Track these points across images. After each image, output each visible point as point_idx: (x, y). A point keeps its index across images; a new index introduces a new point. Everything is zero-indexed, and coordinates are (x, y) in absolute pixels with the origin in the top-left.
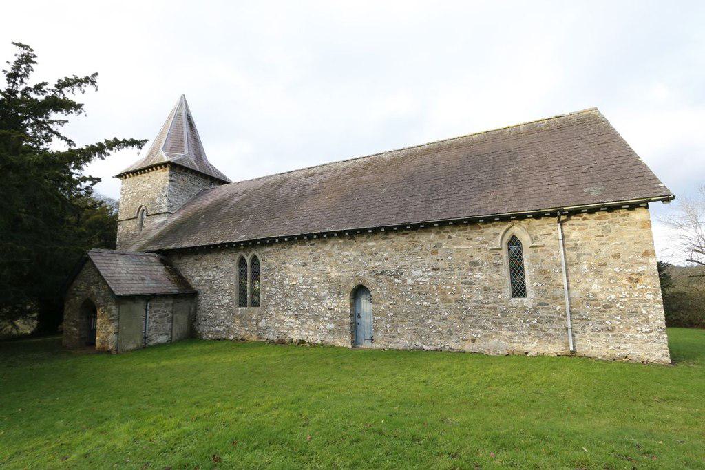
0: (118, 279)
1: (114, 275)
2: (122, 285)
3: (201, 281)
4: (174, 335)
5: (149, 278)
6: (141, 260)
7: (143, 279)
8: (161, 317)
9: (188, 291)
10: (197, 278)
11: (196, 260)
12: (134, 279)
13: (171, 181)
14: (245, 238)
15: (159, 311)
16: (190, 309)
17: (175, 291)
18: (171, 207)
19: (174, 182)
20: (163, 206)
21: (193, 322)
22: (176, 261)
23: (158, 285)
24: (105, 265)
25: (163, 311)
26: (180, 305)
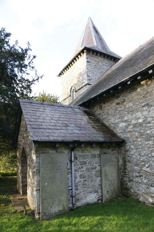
0: (40, 124)
1: (37, 120)
2: (43, 130)
3: (127, 127)
4: (105, 193)
5: (73, 125)
6: (67, 110)
7: (67, 126)
9: (114, 140)
10: (122, 125)
11: (118, 104)
12: (58, 125)
13: (88, 62)
14: (32, 160)
15: (85, 163)
16: (118, 161)
17: (101, 139)
18: (90, 80)
19: (90, 62)
20: (84, 80)
21: (123, 177)
22: (97, 111)
23: (83, 132)
24: (31, 112)
26: (107, 156)
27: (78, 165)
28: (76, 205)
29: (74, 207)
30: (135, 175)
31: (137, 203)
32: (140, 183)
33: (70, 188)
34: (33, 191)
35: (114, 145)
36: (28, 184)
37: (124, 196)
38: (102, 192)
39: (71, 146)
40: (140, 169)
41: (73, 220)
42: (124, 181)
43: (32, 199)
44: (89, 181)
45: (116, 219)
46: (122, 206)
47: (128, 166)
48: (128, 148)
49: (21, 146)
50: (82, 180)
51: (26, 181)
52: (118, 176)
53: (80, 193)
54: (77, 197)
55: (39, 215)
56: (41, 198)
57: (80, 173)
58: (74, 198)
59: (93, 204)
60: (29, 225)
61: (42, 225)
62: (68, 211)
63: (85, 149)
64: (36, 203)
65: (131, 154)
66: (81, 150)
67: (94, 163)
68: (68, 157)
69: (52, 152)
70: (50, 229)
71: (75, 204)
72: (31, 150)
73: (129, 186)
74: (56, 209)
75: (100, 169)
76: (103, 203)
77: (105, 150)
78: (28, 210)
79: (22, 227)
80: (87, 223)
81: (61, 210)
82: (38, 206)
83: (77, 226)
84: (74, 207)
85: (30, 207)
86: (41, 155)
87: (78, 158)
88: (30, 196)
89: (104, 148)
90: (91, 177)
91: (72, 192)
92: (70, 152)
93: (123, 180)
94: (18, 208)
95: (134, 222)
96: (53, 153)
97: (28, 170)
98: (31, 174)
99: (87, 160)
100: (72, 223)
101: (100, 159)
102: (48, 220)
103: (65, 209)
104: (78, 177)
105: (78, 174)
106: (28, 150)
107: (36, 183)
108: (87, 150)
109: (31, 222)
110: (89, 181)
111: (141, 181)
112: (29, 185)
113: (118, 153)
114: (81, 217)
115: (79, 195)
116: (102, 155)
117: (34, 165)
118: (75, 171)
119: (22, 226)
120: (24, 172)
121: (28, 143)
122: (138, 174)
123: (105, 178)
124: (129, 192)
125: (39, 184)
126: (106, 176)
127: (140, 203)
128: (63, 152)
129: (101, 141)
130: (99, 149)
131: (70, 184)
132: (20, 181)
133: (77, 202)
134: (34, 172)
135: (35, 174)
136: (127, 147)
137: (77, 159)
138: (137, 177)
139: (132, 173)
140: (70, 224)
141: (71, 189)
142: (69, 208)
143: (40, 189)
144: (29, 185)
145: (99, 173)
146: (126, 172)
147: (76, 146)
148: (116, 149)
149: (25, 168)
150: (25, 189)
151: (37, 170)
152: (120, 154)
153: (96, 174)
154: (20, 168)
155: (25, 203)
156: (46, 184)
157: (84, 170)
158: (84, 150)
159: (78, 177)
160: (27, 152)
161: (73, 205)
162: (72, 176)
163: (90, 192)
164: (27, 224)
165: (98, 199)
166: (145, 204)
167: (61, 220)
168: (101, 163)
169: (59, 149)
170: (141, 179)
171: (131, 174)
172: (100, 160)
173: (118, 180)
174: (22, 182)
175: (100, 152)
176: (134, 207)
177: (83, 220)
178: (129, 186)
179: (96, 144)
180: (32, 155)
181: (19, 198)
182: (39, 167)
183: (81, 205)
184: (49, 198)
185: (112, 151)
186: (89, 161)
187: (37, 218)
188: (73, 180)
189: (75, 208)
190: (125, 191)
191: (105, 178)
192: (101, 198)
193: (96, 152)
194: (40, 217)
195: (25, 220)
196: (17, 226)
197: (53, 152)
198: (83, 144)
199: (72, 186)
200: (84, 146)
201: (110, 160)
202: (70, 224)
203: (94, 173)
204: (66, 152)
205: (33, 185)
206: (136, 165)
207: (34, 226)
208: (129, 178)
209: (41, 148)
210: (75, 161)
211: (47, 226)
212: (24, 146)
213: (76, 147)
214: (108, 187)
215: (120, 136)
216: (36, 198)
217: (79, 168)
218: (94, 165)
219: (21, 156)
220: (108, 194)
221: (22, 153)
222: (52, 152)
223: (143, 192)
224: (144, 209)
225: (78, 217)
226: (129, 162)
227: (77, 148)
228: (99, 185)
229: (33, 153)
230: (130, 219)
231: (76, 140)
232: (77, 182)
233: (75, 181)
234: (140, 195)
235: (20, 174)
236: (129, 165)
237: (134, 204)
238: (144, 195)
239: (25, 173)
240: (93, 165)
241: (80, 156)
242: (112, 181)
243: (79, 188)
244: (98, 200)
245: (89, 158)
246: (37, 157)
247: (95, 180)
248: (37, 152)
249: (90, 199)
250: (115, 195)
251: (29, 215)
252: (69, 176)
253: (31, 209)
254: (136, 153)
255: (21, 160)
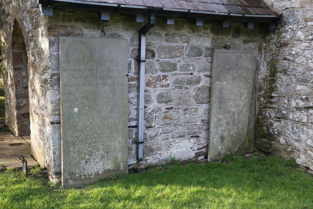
4: (215, 139)
8: (179, 84)
9: (254, 13)
14: (40, 53)
15: (173, 67)
16: (257, 69)
25: (185, 68)
27: (157, 71)
28: (144, 162)
29: (141, 165)
30: (294, 104)
31: (290, 167)
32: (304, 124)
33: (134, 123)
34: (43, 124)
35: (251, 27)
36: (32, 110)
37: (260, 150)
38: (208, 139)
39: (139, 20)
40: (310, 90)
41: (135, 191)
42: (266, 117)
43: (42, 143)
44: (180, 111)
45: (234, 194)
46: (253, 171)
47: (280, 82)
48: (288, 36)
49: (9, 17)
50: (163, 106)
51: (27, 104)
52: (252, 105)
53: (156, 136)
54: (148, 143)
55: (59, 178)
56: (64, 142)
57: (159, 90)
58: (141, 147)
59: (184, 161)
60: (35, 195)
61: (65, 197)
62: (125, 172)
63: (176, 32)
64: (51, 152)
65: (293, 53)
66: (166, 35)
67: (194, 69)
68: (132, 48)
69: (92, 33)
70: (82, 206)
71: (142, 160)
72: (36, 27)
73: (276, 130)
74: (97, 166)
75: (208, 85)
76: (207, 161)
77: (226, 39)
78: (34, 167)
79: (18, 200)
80: (168, 198)
81: (109, 170)
82: (57, 159)
83: (145, 203)
84: (139, 165)
85: (38, 160)
86: (61, 38)
87: (157, 55)
88: (38, 137)
89: (226, 32)
90: (186, 102)
91: (137, 133)
92: (136, 37)
93: (262, 115)
94: (8, 162)
95: (275, 203)
96: (93, 37)
97: (31, 77)
98: (37, 85)
99: (179, 61)
100: (133, 197)
101: (212, 59)
102: (77, 188)
103: (120, 167)
104: (154, 98)
105: (154, 93)
106: (27, 26)
107: (50, 107)
108: (181, 36)
109: (39, 190)
110: (180, 111)
111: (308, 120)
112: (35, 111)
113: (260, 49)
114: (154, 185)
115: (152, 141)
116: (217, 50)
117: (44, 64)
118: (148, 84)
119: (17, 198)
120: (21, 83)
121: (28, 9)
122: (301, 104)
123: (220, 108)
124: (273, 142)
125: (59, 109)
126: (221, 101)
127: (297, 169)
128: (119, 36)
129: (217, 13)
130: (212, 35)
131: (133, 114)
132: (12, 104)
133: (147, 156)
134: (44, 82)
135: (49, 85)
136: (284, 34)
137: (153, 56)
138: (298, 109)
139: (289, 101)
140: (128, 198)
141: (136, 126)
142: (129, 166)
143: (62, 122)
144: (35, 111)
145: (206, 95)
146: (272, 97)
147: (151, 22)
148: (255, 39)
149: (24, 74)
150: (25, 123)
151: (53, 75)
152: (263, 51)
153: (197, 95)
154: (11, 73)
155: (26, 152)
156: (76, 110)
157: (168, 85)
158: (174, 34)
159: (154, 98)
160: (27, 30)
161: (139, 160)
162: (138, 96)
163: (181, 136)
164: (30, 193)
165: (197, 151)
166: (309, 171)
167: (109, 188)
168: (214, 70)
169: (109, 27)
170: (308, 116)
171: (286, 101)
172: (211, 62)
173: (250, 113)
174: (18, 107)
175: (212, 43)
176: (279, 174)
177: (158, 191)
178: (276, 130)
179: (205, 22)
180: (38, 39)
181: (12, 142)
182: (58, 68)
183: (156, 161)
184: (82, 141)
185: (245, 42)
186: (182, 63)
187: (55, 182)
188: (142, 105)
189: (143, 167)
190: (265, 140)
191: (220, 108)
192: (204, 150)
193: (204, 42)
194: (60, 182)
195: (24, 185)
196: (5, 196)
197: (93, 35)
198: (171, 18)
199: (137, 119)
200: (173, 23)
201: (237, 65)
202: (128, 198)
203: (194, 94)
204: (127, 36)
205: (43, 113)
206: (300, 81)
207: (47, 197)
208: (279, 111)
209: (63, 20)
210: (148, 60)
211: (75, 198)
212: (18, 17)
213: (152, 26)
214: (223, 128)
215: (272, 5)
216: (52, 141)
217: (158, 79)
218: (196, 74)
219: (11, 43)
220: (222, 143)
221: (13, 36)
222: (90, 33)
223: (307, 145)
224: (304, 181)
225: (147, 185)
226: (285, 73)
227: (154, 27)
228: (203, 121)
229: (42, 34)
230: (265, 197)
231: (153, 7)
232: (150, 111)
233: (145, 107)
234: (299, 151)
235: (10, 89)
236: (282, 79)
237: (281, 168)
238: (309, 152)
239: (25, 85)
240: (192, 74)
241: (161, 48)
242: (236, 116)
243: (153, 124)
244: (197, 155)
245: (185, 56)
246: (51, 44)
247: (193, 110)
248: (50, 30)
249: (179, 150)
250: (238, 146)
251: (35, 177)
252: (133, 95)
253: (39, 166)
254: (307, 52)
255: (11, 53)
